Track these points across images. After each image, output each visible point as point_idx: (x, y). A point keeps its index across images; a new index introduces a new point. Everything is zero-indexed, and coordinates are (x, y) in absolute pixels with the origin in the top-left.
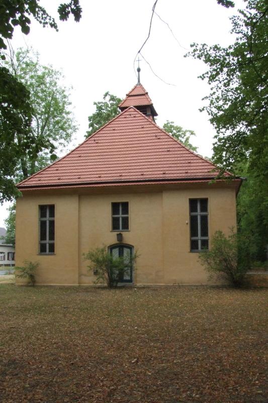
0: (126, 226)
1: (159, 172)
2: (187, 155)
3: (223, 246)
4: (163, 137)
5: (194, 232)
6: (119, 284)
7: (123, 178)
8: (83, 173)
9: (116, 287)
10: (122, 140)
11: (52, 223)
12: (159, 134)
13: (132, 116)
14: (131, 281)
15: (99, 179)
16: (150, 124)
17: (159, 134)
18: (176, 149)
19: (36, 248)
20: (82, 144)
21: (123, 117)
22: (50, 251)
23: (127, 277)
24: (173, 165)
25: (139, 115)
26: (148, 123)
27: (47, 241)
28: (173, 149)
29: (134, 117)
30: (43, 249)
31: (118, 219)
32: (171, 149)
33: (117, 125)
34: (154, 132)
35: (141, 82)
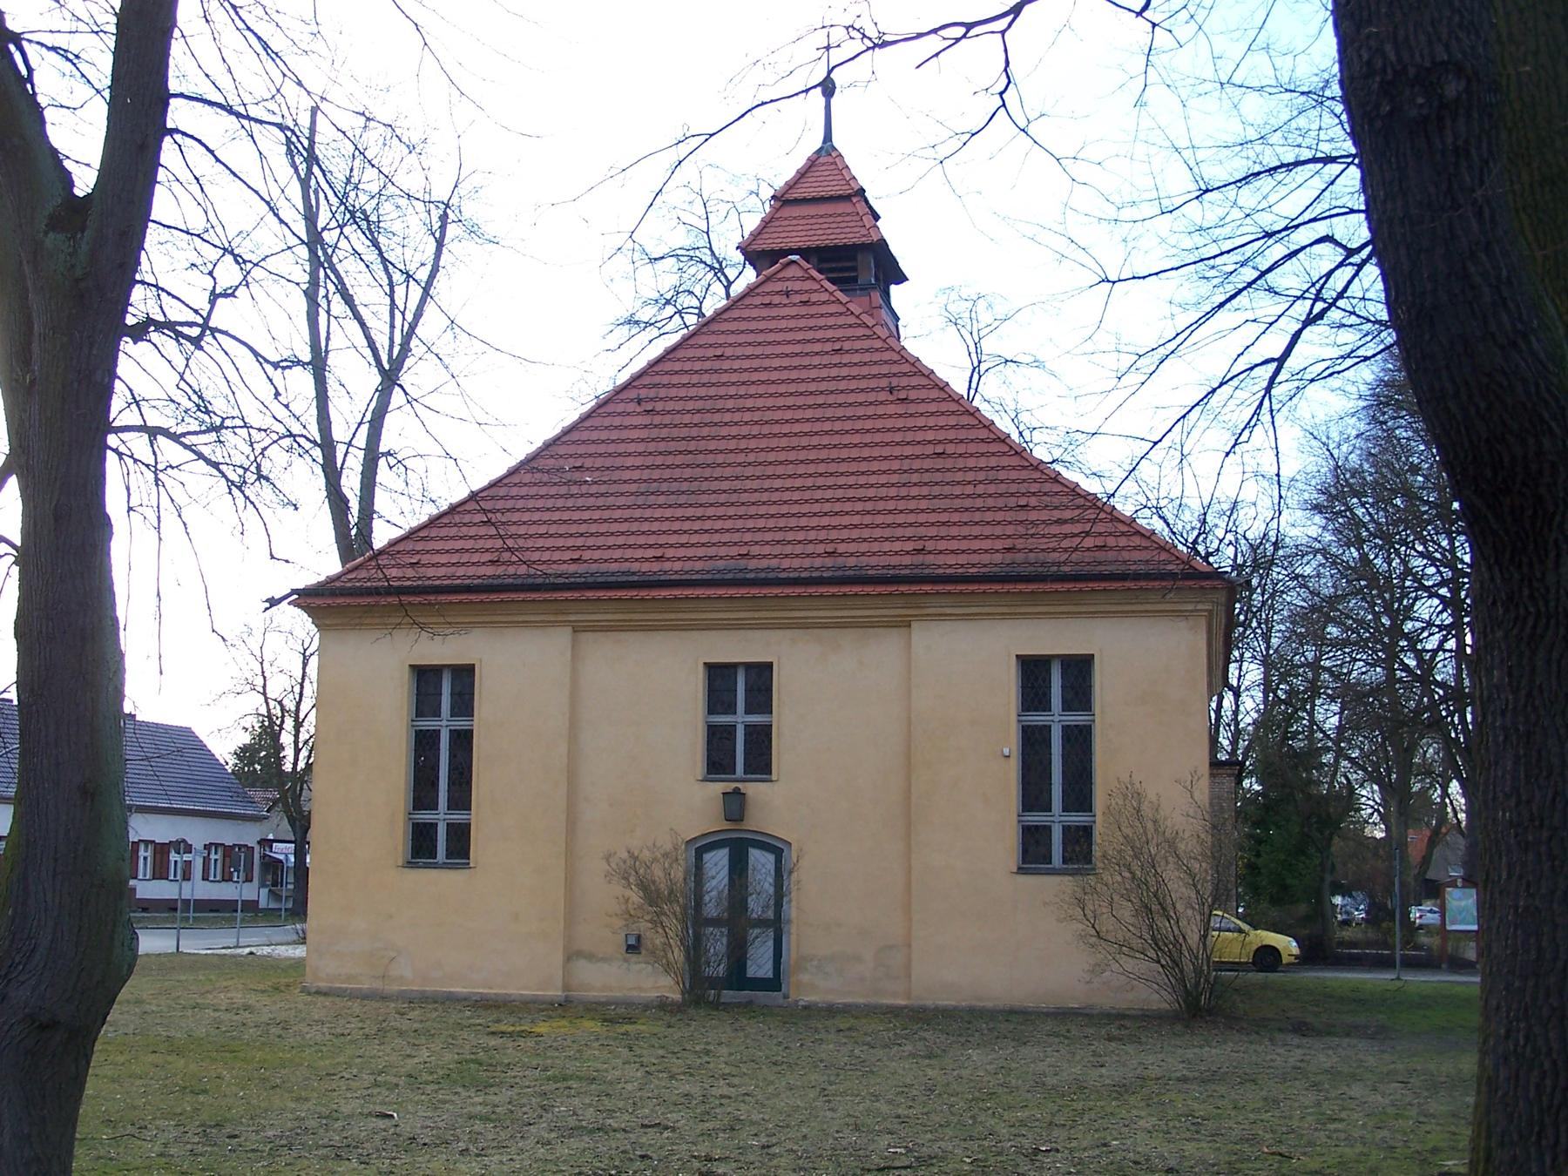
0: (760, 762)
1: (897, 546)
2: (1014, 475)
3: (1308, 861)
4: (923, 394)
5: (1033, 794)
6: (728, 995)
7: (753, 564)
8: (591, 542)
9: (716, 1005)
10: (749, 403)
11: (462, 740)
12: (904, 381)
13: (796, 299)
14: (773, 983)
15: (656, 567)
16: (868, 337)
17: (904, 381)
18: (972, 448)
19: (398, 839)
20: (806, 172)
21: (758, 301)
22: (450, 854)
23: (759, 964)
24: (956, 517)
25: (824, 297)
26: (860, 332)
27: (442, 816)
28: (961, 449)
29: (805, 303)
30: (421, 845)
31: (731, 729)
32: (950, 449)
33: (732, 339)
34: (885, 369)
35: (836, 142)
